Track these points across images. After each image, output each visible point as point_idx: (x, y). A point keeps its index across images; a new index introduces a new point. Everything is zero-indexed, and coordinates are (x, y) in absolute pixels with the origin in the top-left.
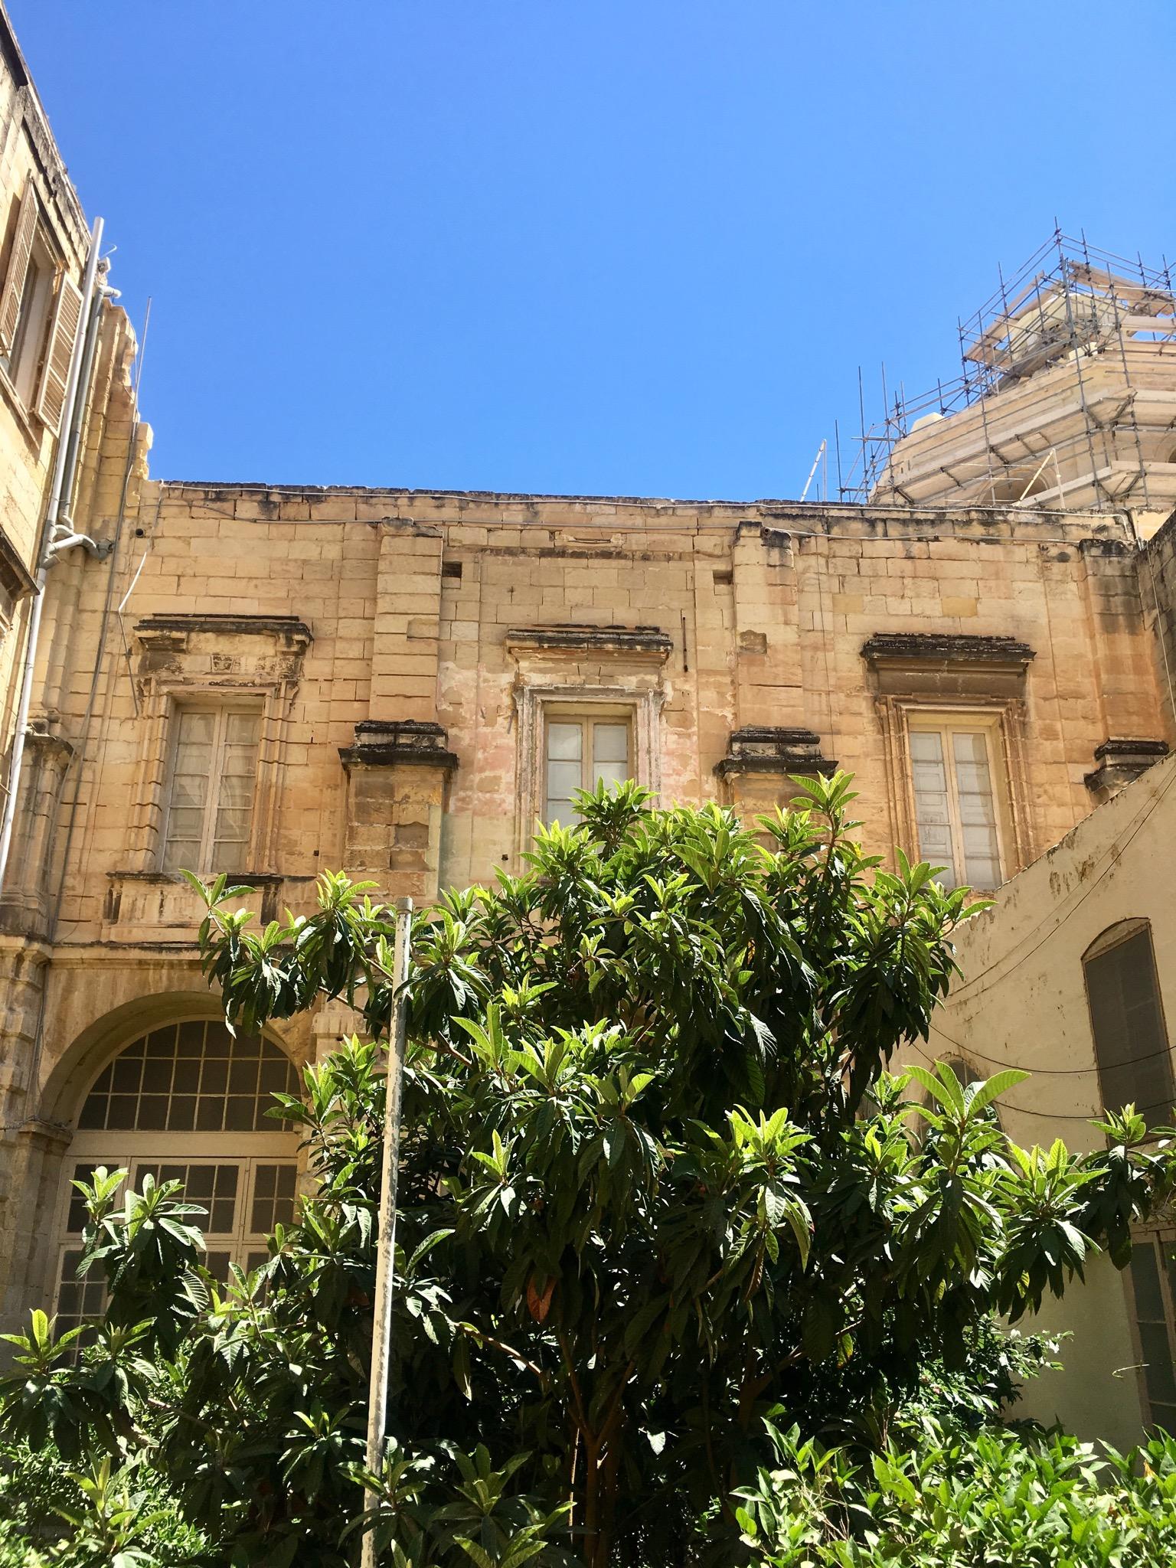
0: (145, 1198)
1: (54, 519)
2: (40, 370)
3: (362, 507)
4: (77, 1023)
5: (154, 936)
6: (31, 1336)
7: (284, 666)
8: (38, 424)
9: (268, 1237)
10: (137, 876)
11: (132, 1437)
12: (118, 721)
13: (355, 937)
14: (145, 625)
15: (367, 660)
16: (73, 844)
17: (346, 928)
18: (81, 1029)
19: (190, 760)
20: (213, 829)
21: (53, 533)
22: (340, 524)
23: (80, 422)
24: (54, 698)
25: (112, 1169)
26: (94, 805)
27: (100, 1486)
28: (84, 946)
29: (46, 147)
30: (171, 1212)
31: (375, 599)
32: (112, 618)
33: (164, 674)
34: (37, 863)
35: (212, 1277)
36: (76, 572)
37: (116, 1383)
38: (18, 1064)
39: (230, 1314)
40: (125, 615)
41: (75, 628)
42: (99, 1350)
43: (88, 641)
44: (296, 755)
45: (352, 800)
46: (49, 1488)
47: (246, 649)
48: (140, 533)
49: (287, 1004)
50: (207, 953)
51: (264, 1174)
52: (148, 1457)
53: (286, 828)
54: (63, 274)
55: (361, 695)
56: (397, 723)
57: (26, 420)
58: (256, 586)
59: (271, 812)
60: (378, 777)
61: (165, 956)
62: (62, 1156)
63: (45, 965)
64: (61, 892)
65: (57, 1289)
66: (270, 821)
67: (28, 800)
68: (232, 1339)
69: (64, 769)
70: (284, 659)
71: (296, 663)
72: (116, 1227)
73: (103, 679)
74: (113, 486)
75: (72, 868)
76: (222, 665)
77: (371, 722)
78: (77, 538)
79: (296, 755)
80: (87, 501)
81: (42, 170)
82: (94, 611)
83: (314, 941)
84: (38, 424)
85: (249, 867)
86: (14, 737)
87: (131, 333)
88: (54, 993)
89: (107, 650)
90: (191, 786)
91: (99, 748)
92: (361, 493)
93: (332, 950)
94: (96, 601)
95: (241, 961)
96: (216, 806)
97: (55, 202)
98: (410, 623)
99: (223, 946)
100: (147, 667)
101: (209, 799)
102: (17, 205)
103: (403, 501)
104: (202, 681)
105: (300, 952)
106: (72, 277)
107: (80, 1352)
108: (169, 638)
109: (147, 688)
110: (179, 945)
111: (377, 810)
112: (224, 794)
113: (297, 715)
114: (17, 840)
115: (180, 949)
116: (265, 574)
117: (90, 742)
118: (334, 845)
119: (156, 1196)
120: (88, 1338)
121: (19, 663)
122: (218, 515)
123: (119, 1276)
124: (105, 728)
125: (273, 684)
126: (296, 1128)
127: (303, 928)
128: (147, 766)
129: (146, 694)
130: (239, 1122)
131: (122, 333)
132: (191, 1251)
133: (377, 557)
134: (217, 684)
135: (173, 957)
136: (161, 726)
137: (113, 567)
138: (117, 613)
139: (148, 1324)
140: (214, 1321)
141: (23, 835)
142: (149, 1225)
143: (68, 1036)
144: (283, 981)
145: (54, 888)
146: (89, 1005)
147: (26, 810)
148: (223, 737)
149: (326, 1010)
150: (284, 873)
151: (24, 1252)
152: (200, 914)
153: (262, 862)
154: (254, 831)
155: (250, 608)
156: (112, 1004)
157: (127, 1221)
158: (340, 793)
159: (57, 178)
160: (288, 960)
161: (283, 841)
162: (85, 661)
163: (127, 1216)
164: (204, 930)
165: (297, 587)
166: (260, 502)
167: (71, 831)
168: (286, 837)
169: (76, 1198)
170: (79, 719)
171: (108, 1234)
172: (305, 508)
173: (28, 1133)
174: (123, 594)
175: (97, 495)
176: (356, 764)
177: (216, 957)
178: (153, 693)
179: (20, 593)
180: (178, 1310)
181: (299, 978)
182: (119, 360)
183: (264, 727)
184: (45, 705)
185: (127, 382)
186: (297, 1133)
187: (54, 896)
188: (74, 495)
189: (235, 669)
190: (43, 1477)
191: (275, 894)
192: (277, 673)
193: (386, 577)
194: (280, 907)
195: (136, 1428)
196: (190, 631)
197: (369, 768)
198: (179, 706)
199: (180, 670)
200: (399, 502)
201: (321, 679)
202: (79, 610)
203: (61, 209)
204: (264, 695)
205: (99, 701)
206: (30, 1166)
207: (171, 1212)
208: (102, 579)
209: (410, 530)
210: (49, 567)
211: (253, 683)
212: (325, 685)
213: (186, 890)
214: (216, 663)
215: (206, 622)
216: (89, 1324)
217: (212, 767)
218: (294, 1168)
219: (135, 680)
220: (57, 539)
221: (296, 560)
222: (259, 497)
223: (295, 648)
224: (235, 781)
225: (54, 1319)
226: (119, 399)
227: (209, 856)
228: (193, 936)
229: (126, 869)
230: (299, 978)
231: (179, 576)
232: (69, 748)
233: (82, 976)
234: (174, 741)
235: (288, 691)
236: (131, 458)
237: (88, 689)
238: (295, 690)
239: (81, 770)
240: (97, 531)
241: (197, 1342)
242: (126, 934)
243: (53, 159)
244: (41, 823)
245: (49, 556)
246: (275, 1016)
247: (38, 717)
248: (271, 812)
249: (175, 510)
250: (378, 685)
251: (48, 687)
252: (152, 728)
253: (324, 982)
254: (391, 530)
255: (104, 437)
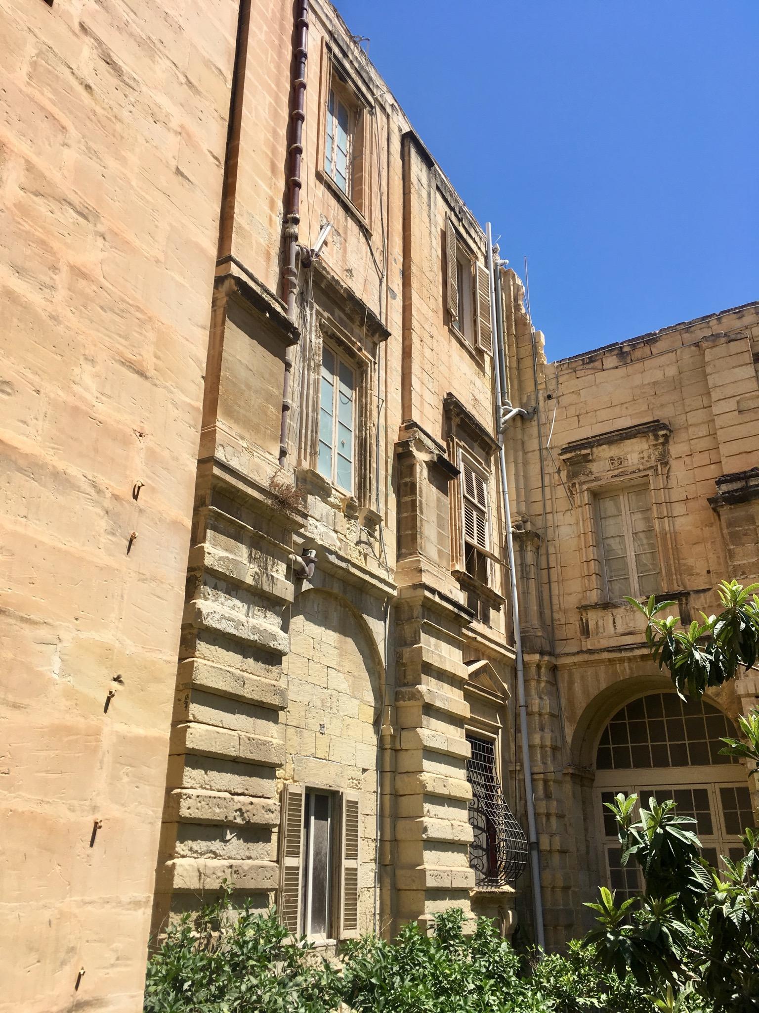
0: (653, 813)
1: (500, 404)
2: (475, 322)
3: (686, 336)
4: (581, 703)
5: (613, 643)
6: (602, 903)
7: (657, 453)
8: (480, 353)
9: (741, 837)
10: (595, 606)
11: (680, 972)
12: (562, 513)
13: (755, 624)
14: (565, 451)
15: (713, 435)
16: (553, 593)
17: (747, 618)
18: (584, 705)
19: (611, 526)
20: (635, 568)
21: (502, 412)
22: (672, 352)
23: (503, 344)
24: (523, 508)
25: (626, 795)
26: (559, 567)
27: (669, 1005)
28: (574, 654)
29: (452, 196)
30: (672, 822)
31: (709, 393)
32: (545, 452)
33: (582, 478)
34: (535, 608)
35: (710, 865)
36: (519, 431)
37: (662, 937)
38: (552, 731)
39: (728, 891)
40: (552, 448)
41: (525, 464)
42: (646, 913)
43: (534, 469)
44: (679, 509)
45: (725, 531)
46: (633, 1003)
47: (630, 449)
48: (549, 397)
49: (717, 676)
50: (653, 649)
51: (726, 794)
52: (694, 987)
53: (683, 559)
54: (475, 263)
55: (714, 459)
56: (745, 472)
57: (474, 353)
58: (627, 408)
59: (671, 551)
60: (740, 512)
61: (624, 654)
62: (591, 787)
63: (554, 669)
64: (553, 623)
65: (608, 873)
66: (671, 556)
67: (522, 571)
68: (735, 908)
69: (538, 548)
70: (656, 449)
71: (664, 450)
72: (639, 833)
73: (547, 490)
74: (528, 375)
75: (555, 608)
76: (616, 463)
77: (726, 476)
78: (515, 411)
79: (679, 509)
80: (516, 388)
81: (452, 209)
82: (534, 451)
83: (726, 631)
84: (480, 353)
85: (665, 588)
86: (506, 536)
87: (519, 282)
88: (563, 686)
89: (546, 472)
90: (614, 544)
91: (554, 532)
92: (682, 327)
93: (740, 636)
94: (534, 444)
95: (678, 651)
96: (633, 554)
97: (463, 224)
98: (738, 402)
99: (663, 641)
100: (572, 476)
101: (628, 550)
102: (444, 234)
103: (713, 322)
104: (606, 477)
105: (717, 639)
106: (481, 263)
107: (632, 914)
108: (581, 455)
109: (574, 489)
110: (631, 646)
111: (746, 535)
112: (636, 545)
113: (673, 483)
114: (521, 596)
115: (632, 649)
116: (631, 398)
117: (548, 529)
118: (720, 564)
119: (660, 812)
120: (636, 906)
121: (500, 493)
122: (593, 372)
123: (648, 865)
124: (555, 518)
125: (651, 467)
126: (741, 761)
127: (715, 623)
128: (585, 537)
129: (574, 493)
130: (700, 760)
131: (514, 283)
132: (692, 848)
133: (704, 365)
134: (616, 476)
135: (629, 654)
136: (588, 510)
137: (538, 422)
138: (547, 448)
139: (675, 897)
140: (720, 896)
141: (524, 593)
142: (659, 830)
143: (578, 712)
144: (710, 661)
145: (548, 622)
146: (585, 691)
147: (522, 577)
148: (627, 508)
149: (742, 677)
150: (689, 589)
151: (583, 849)
152: (640, 623)
153: (673, 584)
154: (662, 564)
155: (626, 422)
156: (599, 689)
157: (645, 828)
158: (715, 529)
159: (461, 209)
160: (710, 646)
161: (683, 568)
162: (536, 482)
163: (644, 825)
164: (648, 633)
165: (653, 401)
166: (617, 355)
167: (550, 585)
168: (684, 565)
169: (606, 814)
170: (540, 517)
171: (634, 837)
172: (647, 350)
173: (568, 774)
174: (547, 436)
175: (520, 382)
176: (722, 506)
177: (661, 651)
178: (578, 491)
179: (491, 452)
180: (693, 888)
181: (721, 657)
182: (516, 300)
183: (653, 497)
184: (519, 513)
185: (523, 311)
186: (743, 764)
187: (549, 627)
188: (508, 387)
189: (625, 463)
190: (627, 995)
191: (687, 604)
192: (653, 459)
193: (713, 376)
194: (692, 612)
195: (683, 967)
196: (592, 447)
197: (732, 507)
198: (596, 495)
199: (591, 472)
200: (711, 324)
201: (683, 455)
202: (525, 453)
203: (467, 227)
204: (647, 475)
205: (548, 503)
206: (574, 794)
207: (672, 822)
208: (534, 431)
209: (723, 340)
210: (504, 432)
211: (639, 469)
212: (687, 459)
213: (627, 611)
214: (612, 463)
215: (600, 439)
216: (637, 897)
217: (625, 528)
218: (747, 789)
219: (566, 486)
220: (504, 415)
221: (649, 384)
222: (616, 352)
223: (661, 440)
224: (641, 535)
225: (614, 894)
226: (521, 323)
227: (637, 586)
228: (642, 638)
229: (588, 603)
230: (721, 657)
231: (578, 416)
232: (537, 536)
233: (577, 674)
234: (598, 518)
235: (663, 469)
236: (535, 354)
237: (540, 498)
238: (667, 468)
239: (547, 547)
240: (525, 404)
241: (711, 910)
242: (596, 643)
243: (456, 200)
244: (532, 583)
245: (502, 426)
246: (710, 685)
247: (516, 521)
248: (671, 551)
249: (567, 377)
250: (724, 450)
251: (518, 503)
252: (582, 513)
253: (740, 658)
254: (710, 344)
255: (517, 347)
